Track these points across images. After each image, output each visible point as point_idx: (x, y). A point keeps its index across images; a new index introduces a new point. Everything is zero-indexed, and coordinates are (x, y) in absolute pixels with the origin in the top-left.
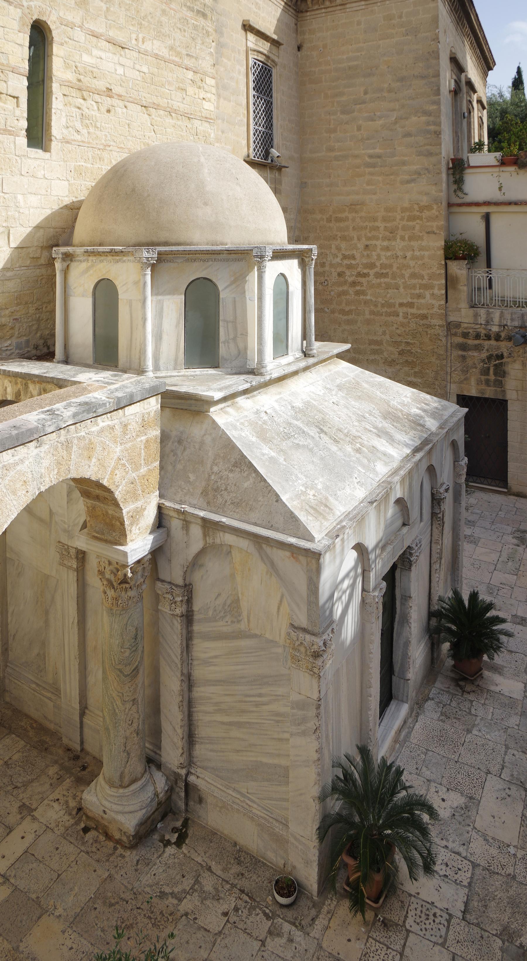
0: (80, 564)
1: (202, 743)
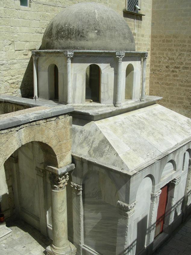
0: (44, 175)
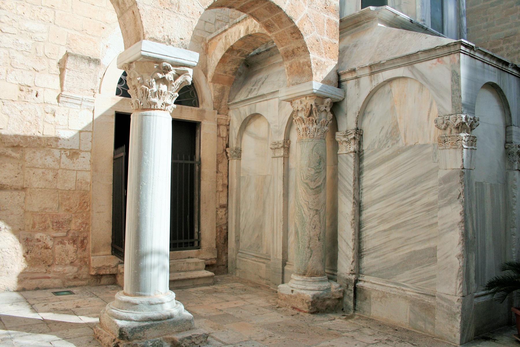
0: (286, 153)
1: (368, 254)
